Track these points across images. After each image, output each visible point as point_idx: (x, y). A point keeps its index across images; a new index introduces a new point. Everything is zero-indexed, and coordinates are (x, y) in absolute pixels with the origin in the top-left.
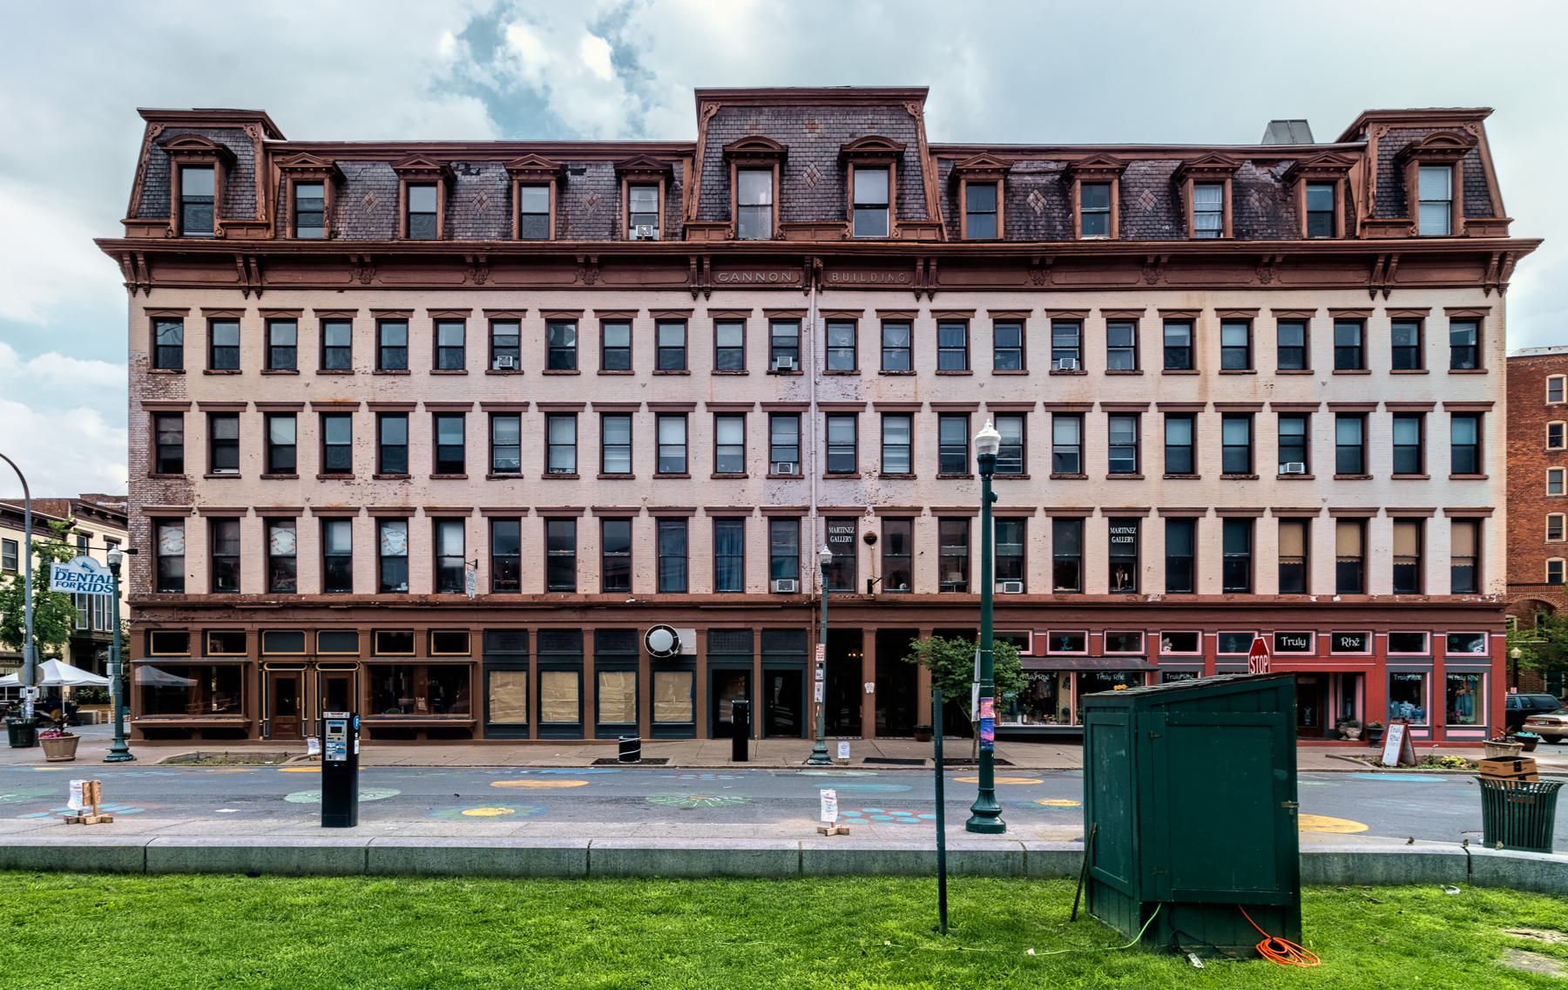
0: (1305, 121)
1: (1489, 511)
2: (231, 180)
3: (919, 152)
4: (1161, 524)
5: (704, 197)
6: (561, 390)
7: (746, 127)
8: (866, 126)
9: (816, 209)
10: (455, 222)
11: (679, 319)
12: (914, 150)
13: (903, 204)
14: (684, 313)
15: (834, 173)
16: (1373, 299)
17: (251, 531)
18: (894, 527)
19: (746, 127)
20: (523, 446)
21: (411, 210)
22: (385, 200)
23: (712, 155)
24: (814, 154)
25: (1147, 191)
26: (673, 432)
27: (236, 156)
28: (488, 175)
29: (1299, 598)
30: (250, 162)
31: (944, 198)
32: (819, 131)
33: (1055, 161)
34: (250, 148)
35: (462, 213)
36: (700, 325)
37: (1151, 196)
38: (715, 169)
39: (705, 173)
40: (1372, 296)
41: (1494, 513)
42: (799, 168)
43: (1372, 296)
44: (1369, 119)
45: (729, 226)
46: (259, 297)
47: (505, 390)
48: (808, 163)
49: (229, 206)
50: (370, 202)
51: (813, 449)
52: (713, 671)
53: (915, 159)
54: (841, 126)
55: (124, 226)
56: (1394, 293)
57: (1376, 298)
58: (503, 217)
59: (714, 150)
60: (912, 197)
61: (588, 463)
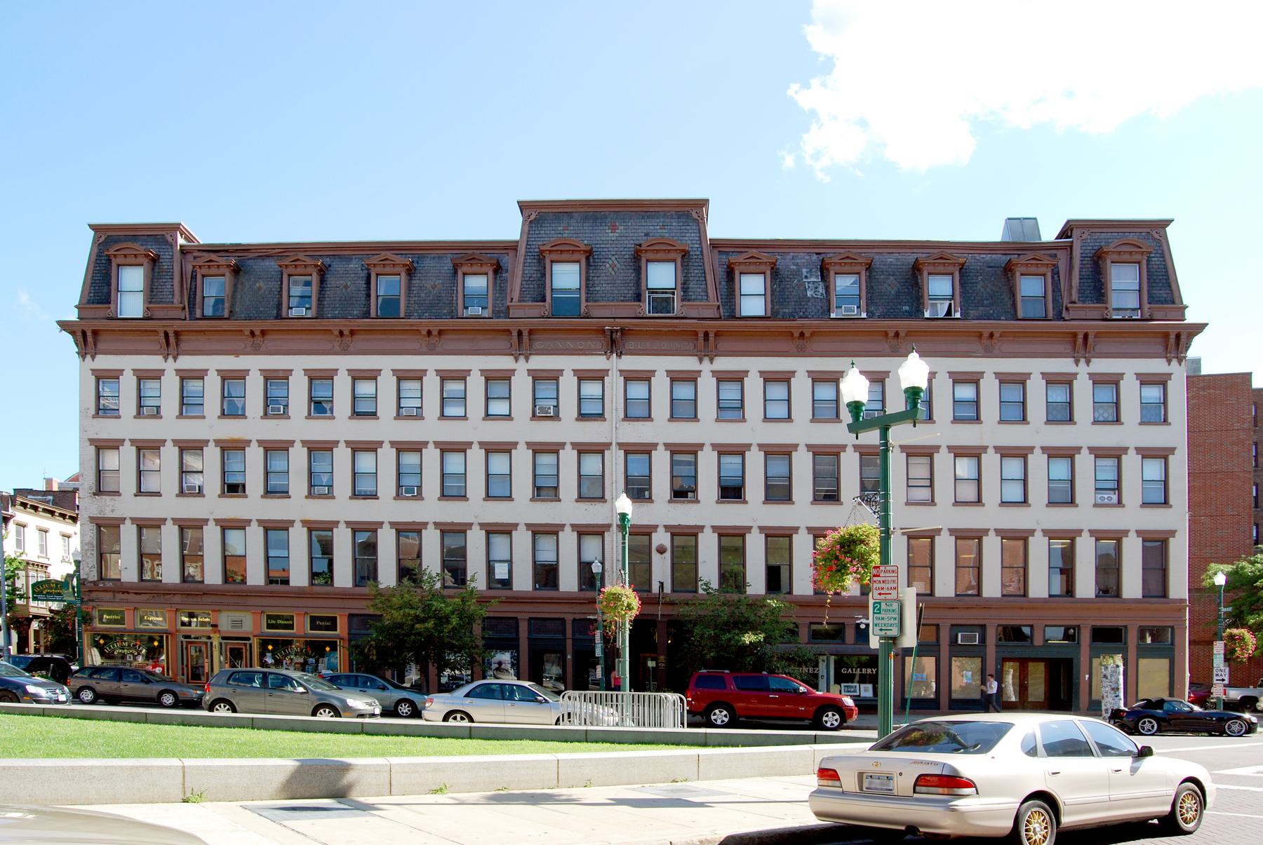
0: (1035, 219)
1: (1172, 533)
2: (156, 274)
3: (701, 247)
4: (1138, 542)
5: (525, 282)
6: (320, 430)
7: (559, 228)
8: (658, 227)
9: (616, 292)
10: (325, 303)
11: (691, 378)
12: (698, 246)
13: (324, 287)
14: (556, 373)
15: (631, 264)
16: (1077, 365)
17: (211, 535)
18: (680, 541)
19: (559, 228)
22: (271, 286)
23: (532, 250)
24: (615, 249)
26: (499, 464)
28: (352, 266)
29: (552, 594)
30: (170, 260)
31: (724, 283)
33: (817, 254)
34: (170, 250)
35: (331, 296)
36: (707, 385)
37: (895, 282)
38: (534, 261)
39: (526, 264)
40: (1077, 363)
42: (602, 260)
43: (1077, 363)
47: (275, 430)
48: (610, 256)
49: (155, 293)
50: (260, 289)
51: (614, 479)
53: (698, 253)
54: (637, 227)
55: (77, 310)
58: (363, 299)
59: (533, 247)
60: (695, 282)
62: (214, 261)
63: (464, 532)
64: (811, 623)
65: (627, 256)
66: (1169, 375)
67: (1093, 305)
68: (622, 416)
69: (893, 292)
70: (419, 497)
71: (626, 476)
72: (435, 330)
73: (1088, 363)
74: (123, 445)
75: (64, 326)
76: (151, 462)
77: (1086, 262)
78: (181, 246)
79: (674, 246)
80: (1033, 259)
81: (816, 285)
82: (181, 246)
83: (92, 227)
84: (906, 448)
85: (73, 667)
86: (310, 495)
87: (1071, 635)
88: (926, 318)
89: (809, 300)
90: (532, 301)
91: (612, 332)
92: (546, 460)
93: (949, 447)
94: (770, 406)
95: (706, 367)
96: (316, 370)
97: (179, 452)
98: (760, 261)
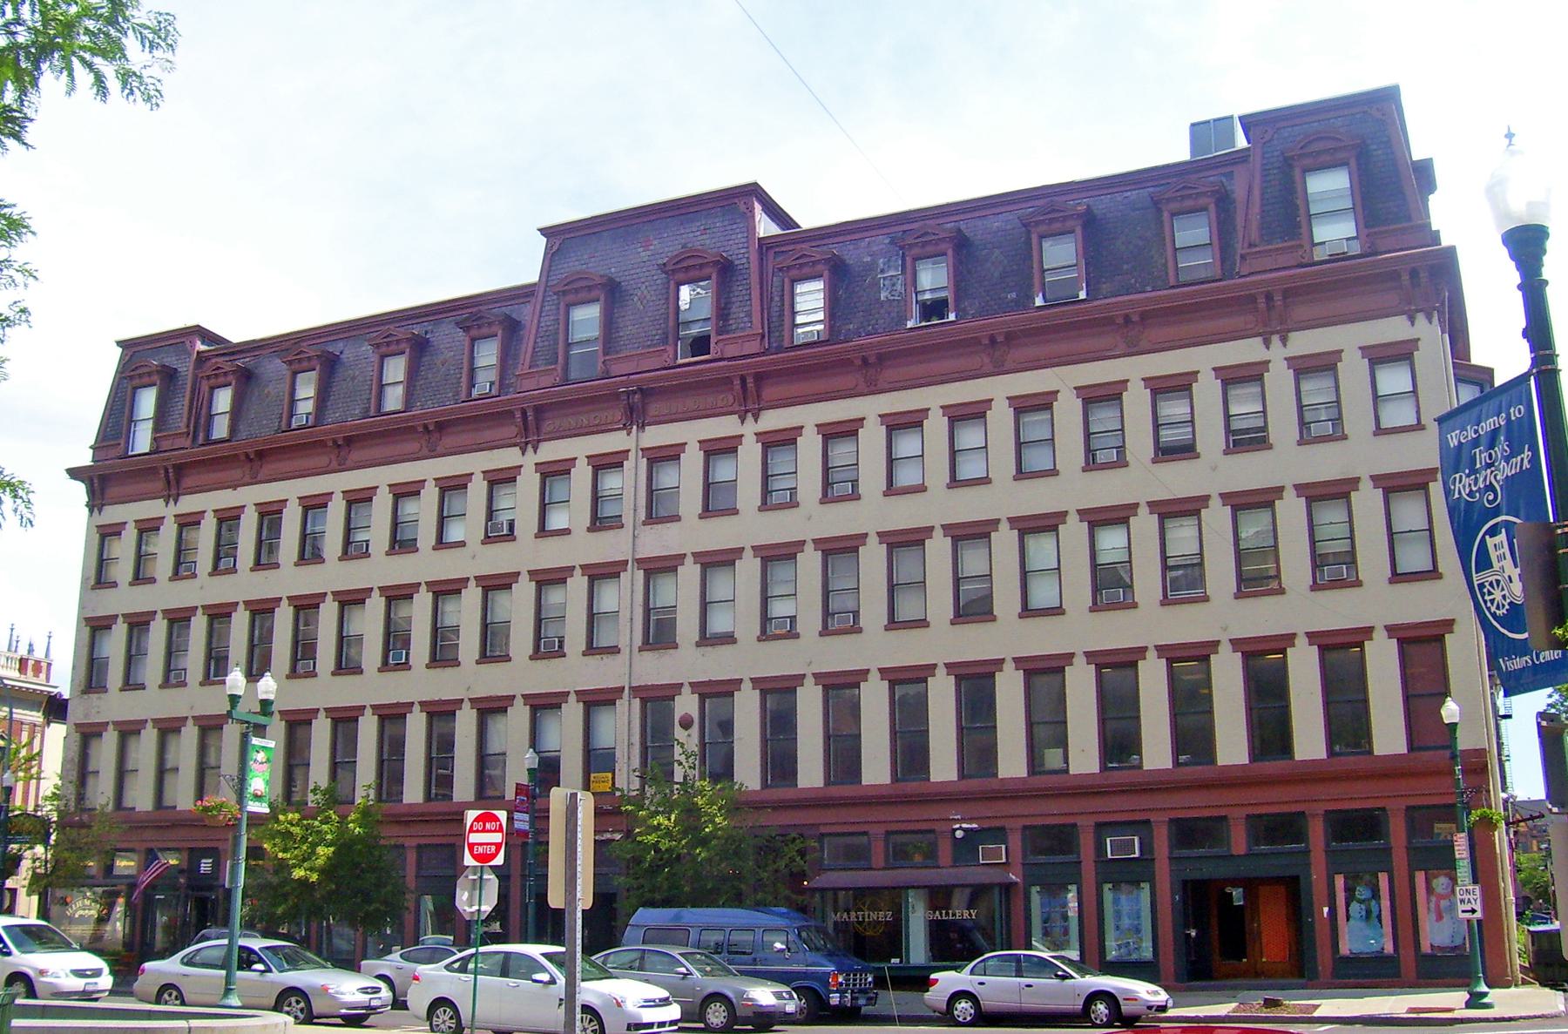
8: (698, 233)
14: (416, 485)
16: (1268, 348)
20: (1062, 569)
21: (1046, 267)
25: (997, 252)
27: (732, 262)
32: (652, 247)
40: (1267, 344)
41: (1456, 627)
43: (1267, 344)
44: (199, 332)
45: (1301, 246)
46: (756, 421)
52: (1185, 883)
53: (745, 261)
56: (1293, 336)
57: (1272, 346)
61: (873, 611)
62: (1058, 211)
63: (1061, 670)
64: (888, 833)
65: (659, 282)
66: (1414, 342)
67: (1285, 244)
68: (642, 515)
69: (996, 274)
70: (856, 629)
71: (1094, 565)
72: (431, 423)
73: (1284, 341)
74: (1281, 498)
75: (74, 473)
76: (721, 585)
77: (1271, 177)
78: (198, 352)
79: (1340, 140)
80: (1184, 188)
81: (895, 279)
82: (198, 352)
83: (119, 343)
84: (761, 550)
85: (952, 935)
86: (825, 631)
87: (963, 838)
88: (1038, 307)
89: (882, 304)
90: (546, 365)
91: (628, 393)
92: (1330, 515)
93: (1222, 495)
94: (1027, 454)
95: (1277, 355)
96: (716, 439)
97: (483, 593)
98: (813, 259)
